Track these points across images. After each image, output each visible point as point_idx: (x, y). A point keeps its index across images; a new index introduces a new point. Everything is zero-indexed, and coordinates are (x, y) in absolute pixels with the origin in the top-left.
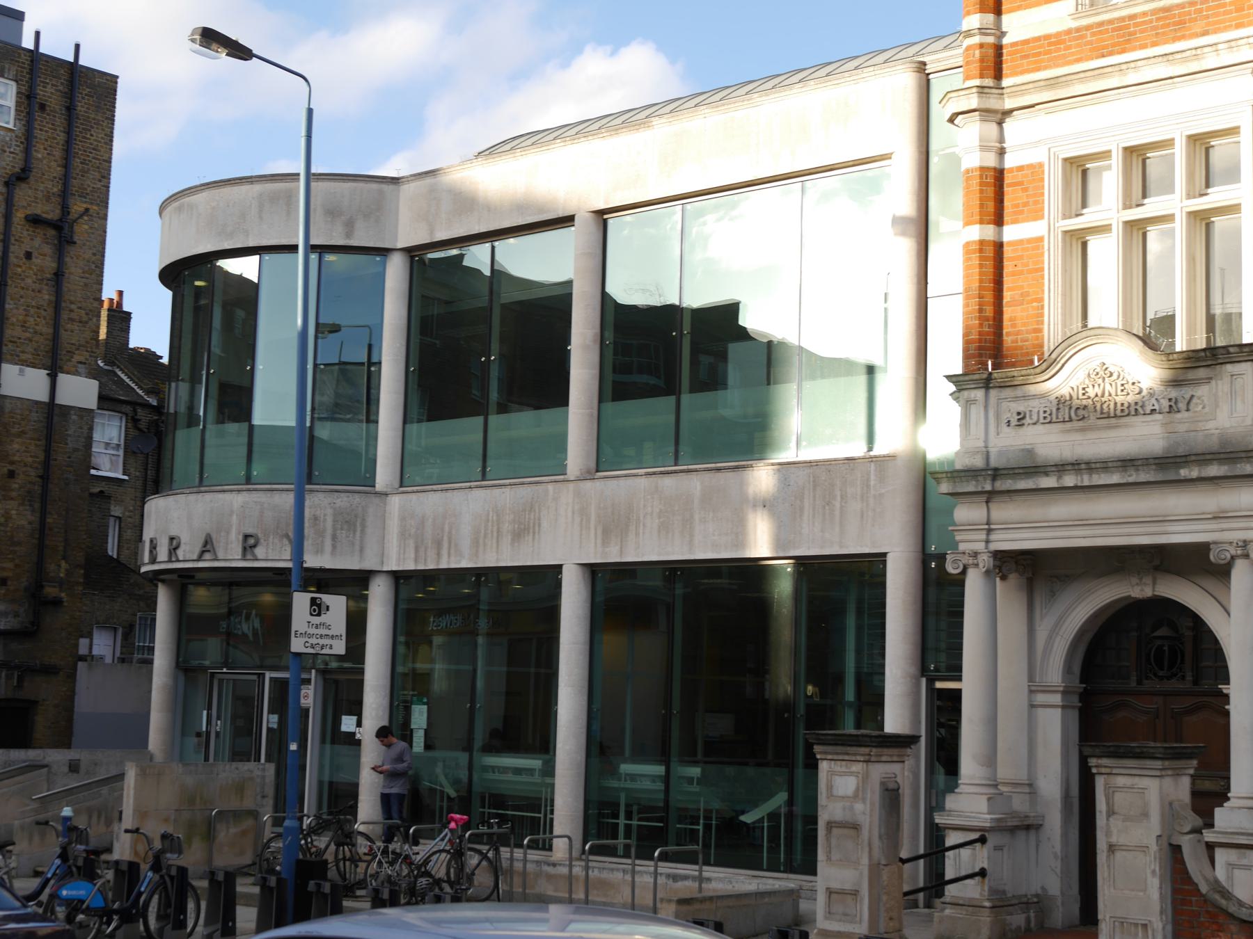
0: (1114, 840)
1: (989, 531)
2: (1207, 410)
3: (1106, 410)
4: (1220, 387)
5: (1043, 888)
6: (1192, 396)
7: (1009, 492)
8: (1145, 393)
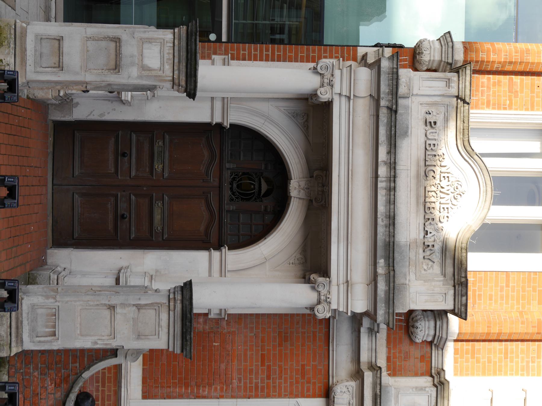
0: (118, 310)
1: (349, 98)
2: (423, 272)
3: (431, 194)
4: (438, 283)
5: (77, 104)
6: (434, 262)
7: (378, 116)
8: (440, 225)
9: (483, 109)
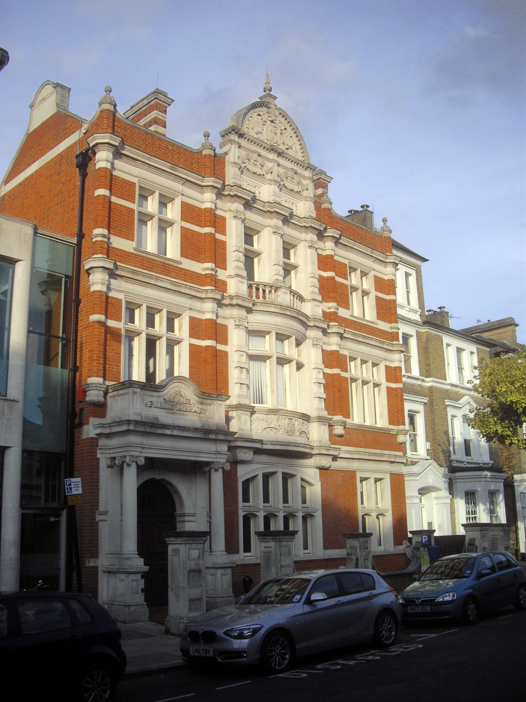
9: (120, 369)
